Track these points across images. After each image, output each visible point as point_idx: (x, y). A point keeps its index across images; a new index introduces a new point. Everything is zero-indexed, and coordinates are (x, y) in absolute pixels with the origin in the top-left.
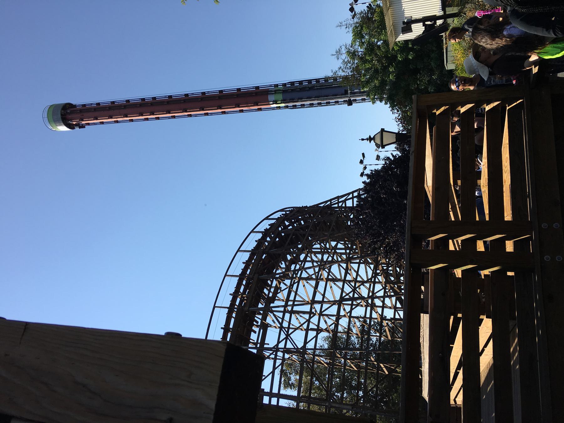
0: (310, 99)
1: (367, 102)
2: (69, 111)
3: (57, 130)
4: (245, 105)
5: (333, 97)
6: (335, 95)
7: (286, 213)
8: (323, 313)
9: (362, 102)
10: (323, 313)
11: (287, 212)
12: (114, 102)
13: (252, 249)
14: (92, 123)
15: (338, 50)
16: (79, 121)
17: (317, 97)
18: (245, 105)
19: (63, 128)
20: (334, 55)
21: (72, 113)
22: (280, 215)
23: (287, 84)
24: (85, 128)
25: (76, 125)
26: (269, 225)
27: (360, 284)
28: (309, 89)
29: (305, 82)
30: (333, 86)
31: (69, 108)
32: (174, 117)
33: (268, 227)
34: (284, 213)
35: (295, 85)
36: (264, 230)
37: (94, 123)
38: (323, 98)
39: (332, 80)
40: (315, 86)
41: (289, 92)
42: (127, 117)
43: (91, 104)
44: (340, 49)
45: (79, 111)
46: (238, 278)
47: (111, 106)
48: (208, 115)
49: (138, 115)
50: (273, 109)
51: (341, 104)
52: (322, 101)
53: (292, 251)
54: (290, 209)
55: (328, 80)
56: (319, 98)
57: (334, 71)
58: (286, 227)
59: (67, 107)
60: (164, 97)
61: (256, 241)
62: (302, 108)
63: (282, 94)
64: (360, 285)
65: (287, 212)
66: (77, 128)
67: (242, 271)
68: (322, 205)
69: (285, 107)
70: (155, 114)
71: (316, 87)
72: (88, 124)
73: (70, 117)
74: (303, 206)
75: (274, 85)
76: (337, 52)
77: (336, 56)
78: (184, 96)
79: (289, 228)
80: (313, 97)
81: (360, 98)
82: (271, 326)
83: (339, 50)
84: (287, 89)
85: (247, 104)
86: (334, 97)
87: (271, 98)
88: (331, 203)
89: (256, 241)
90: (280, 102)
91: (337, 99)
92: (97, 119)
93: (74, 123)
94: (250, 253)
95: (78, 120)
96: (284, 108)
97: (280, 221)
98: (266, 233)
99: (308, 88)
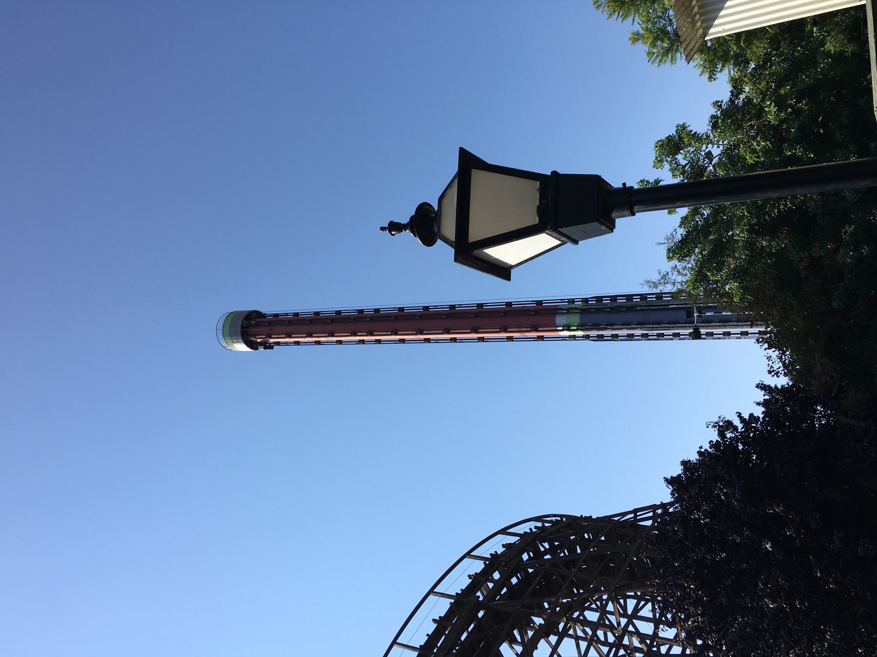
0: (628, 327)
1: (734, 339)
2: (253, 322)
3: (234, 349)
4: (517, 329)
5: (669, 326)
6: (673, 323)
7: (543, 525)
9: (725, 339)
11: (547, 525)
12: (319, 312)
13: (457, 593)
14: (284, 343)
16: (266, 338)
21: (257, 325)
22: (531, 529)
23: (589, 299)
24: (273, 349)
25: (261, 344)
26: (504, 546)
28: (611, 309)
29: (621, 298)
30: (671, 306)
31: (256, 318)
33: (500, 550)
34: (539, 524)
35: (603, 302)
36: (491, 554)
37: (286, 343)
38: (651, 326)
39: (670, 297)
41: (592, 312)
42: (333, 336)
45: (329, 321)
47: (449, 312)
49: (349, 334)
50: (564, 338)
52: (650, 332)
53: (576, 592)
54: (554, 519)
55: (662, 297)
58: (539, 555)
60: (531, 302)
62: (613, 340)
63: (579, 315)
65: (547, 525)
66: (261, 348)
68: (616, 519)
69: (583, 337)
70: (374, 334)
71: (640, 306)
72: (278, 344)
73: (253, 330)
74: (582, 516)
75: (567, 301)
78: (373, 311)
79: (546, 557)
80: (634, 323)
81: (721, 331)
84: (590, 307)
85: (520, 328)
86: (672, 325)
87: (560, 320)
88: (636, 516)
89: (470, 576)
90: (575, 328)
92: (290, 337)
93: (259, 340)
94: (453, 601)
95: (264, 337)
96: (582, 339)
97: (528, 541)
98: (493, 562)
99: (624, 307)
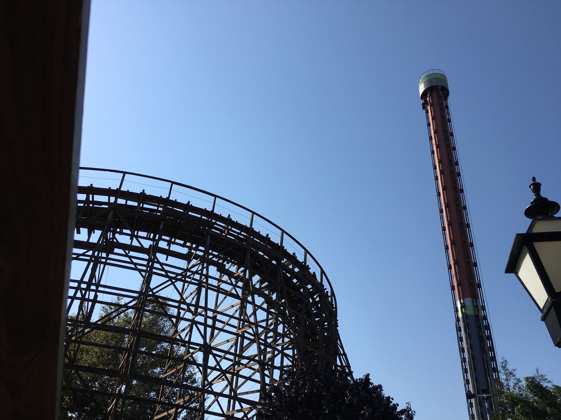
0: (470, 349)
4: (457, 271)
6: (476, 380)
8: (194, 325)
9: (469, 415)
10: (194, 325)
11: (330, 299)
13: (284, 247)
14: (428, 116)
15: (545, 377)
17: (473, 358)
18: (457, 271)
19: (422, 89)
20: (538, 373)
22: (326, 289)
23: (486, 321)
24: (423, 109)
25: (426, 101)
26: (314, 273)
27: (230, 380)
29: (491, 343)
30: (489, 378)
32: (439, 195)
34: (329, 294)
36: (308, 265)
37: (428, 118)
38: (472, 364)
40: (487, 355)
43: (449, 113)
44: (547, 381)
46: (248, 226)
48: (443, 230)
51: (465, 387)
52: (468, 364)
54: (334, 303)
56: (471, 359)
57: (515, 373)
58: (311, 295)
59: (444, 92)
61: (294, 254)
64: (227, 379)
65: (330, 299)
66: (423, 102)
67: (258, 231)
68: (339, 342)
71: (486, 356)
72: (427, 112)
73: (435, 94)
74: (338, 320)
76: (542, 376)
77: (537, 375)
80: (473, 352)
82: (189, 264)
83: (545, 379)
87: (468, 301)
89: (294, 254)
90: (464, 311)
91: (472, 383)
93: (428, 99)
94: (279, 245)
95: (431, 102)
96: (456, 316)
97: (319, 288)
98: (304, 267)
